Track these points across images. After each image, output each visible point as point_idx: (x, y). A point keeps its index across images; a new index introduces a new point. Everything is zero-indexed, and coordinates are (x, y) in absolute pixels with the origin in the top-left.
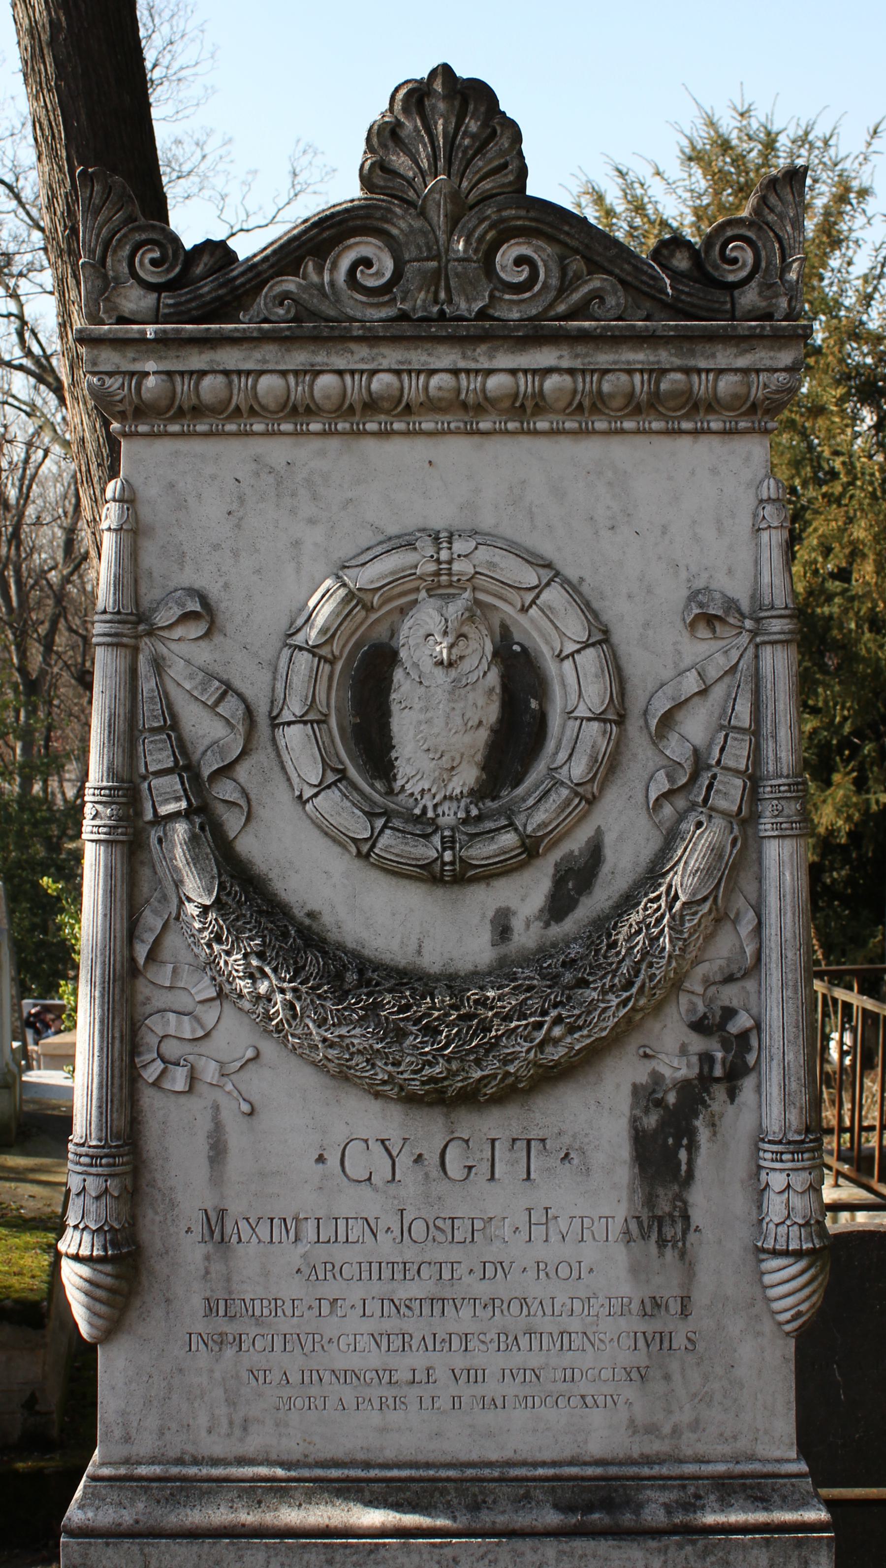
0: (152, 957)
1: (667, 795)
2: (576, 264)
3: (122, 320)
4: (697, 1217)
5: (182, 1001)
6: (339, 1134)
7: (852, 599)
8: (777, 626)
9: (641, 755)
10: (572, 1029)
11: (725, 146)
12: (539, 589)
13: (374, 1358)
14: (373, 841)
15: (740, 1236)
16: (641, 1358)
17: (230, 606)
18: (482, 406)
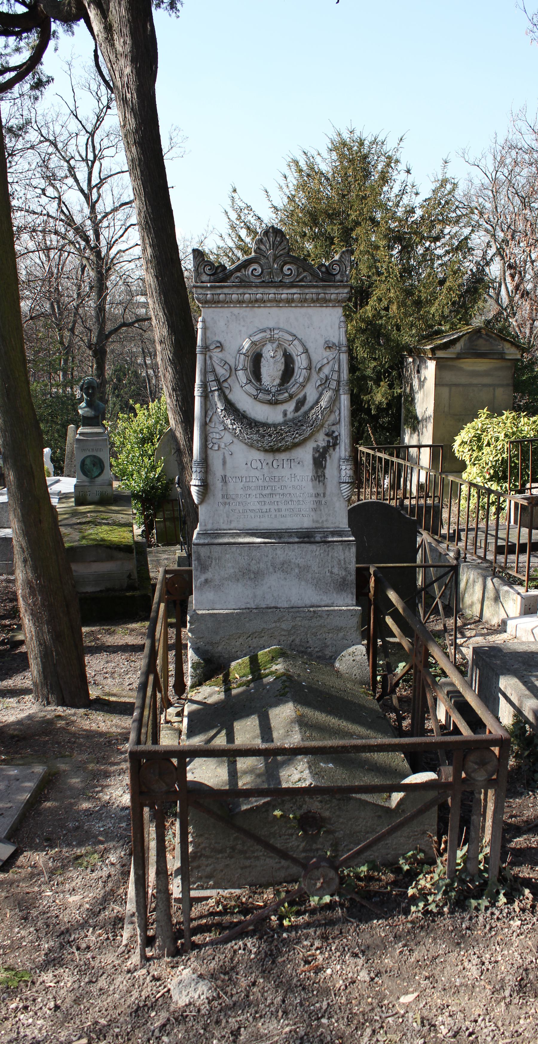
0: (210, 421)
1: (320, 385)
2: (301, 270)
3: (202, 282)
4: (327, 476)
5: (216, 430)
6: (250, 458)
7: (389, 318)
8: (344, 349)
9: (315, 376)
10: (300, 435)
11: (344, 144)
12: (293, 341)
13: (258, 507)
14: (258, 395)
15: (335, 481)
16: (315, 506)
17: (226, 345)
18: (280, 301)
